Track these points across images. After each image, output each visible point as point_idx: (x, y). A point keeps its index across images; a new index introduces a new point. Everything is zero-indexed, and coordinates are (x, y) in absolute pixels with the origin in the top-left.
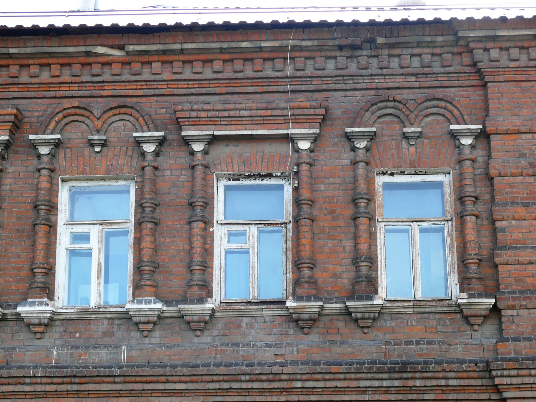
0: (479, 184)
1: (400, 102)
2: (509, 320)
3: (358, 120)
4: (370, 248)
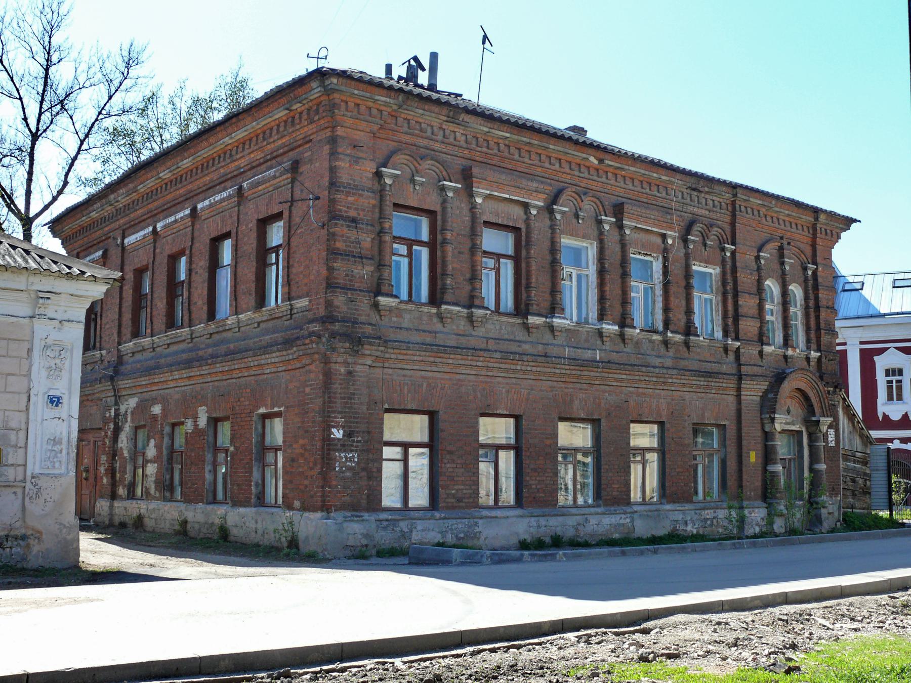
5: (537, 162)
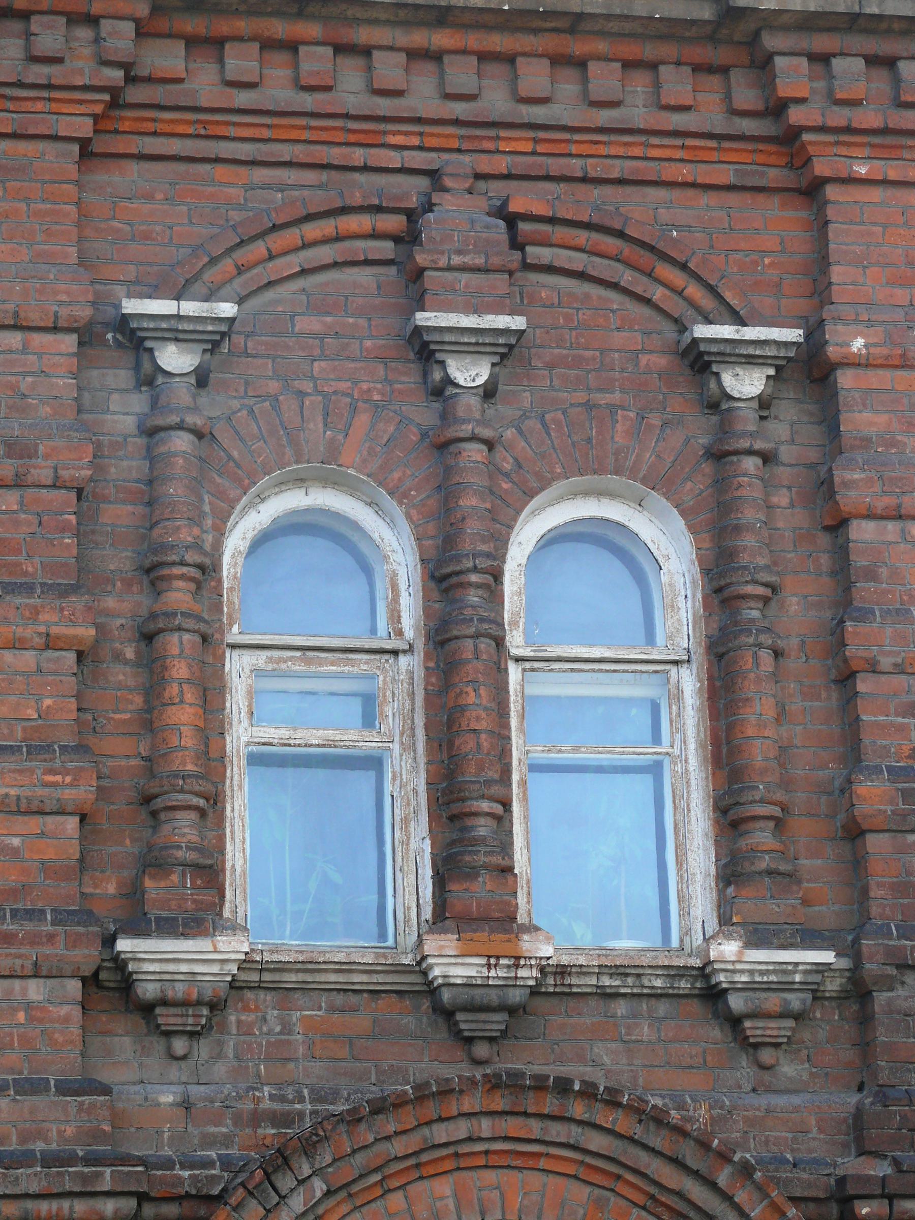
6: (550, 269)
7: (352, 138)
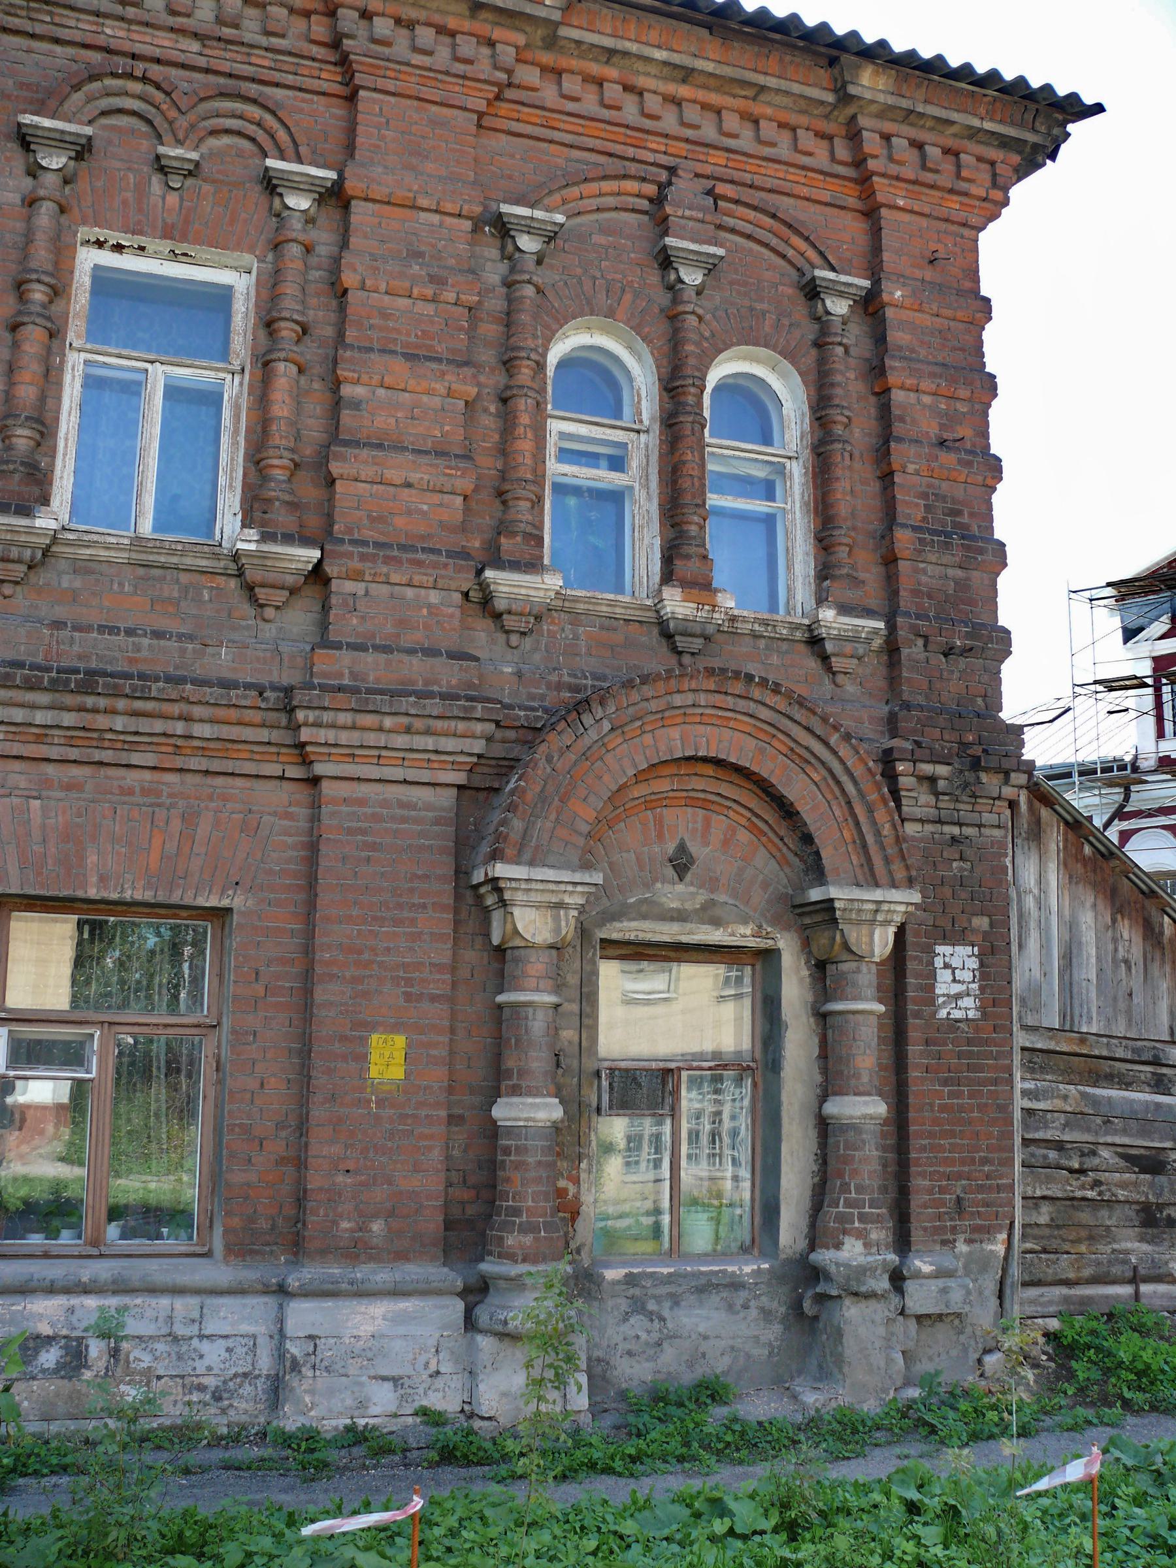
0: (313, 301)
1: (158, 87)
2: (345, 604)
3: (52, 103)
4: (42, 398)
5: (945, 180)
6: (733, 231)
7: (629, 141)
